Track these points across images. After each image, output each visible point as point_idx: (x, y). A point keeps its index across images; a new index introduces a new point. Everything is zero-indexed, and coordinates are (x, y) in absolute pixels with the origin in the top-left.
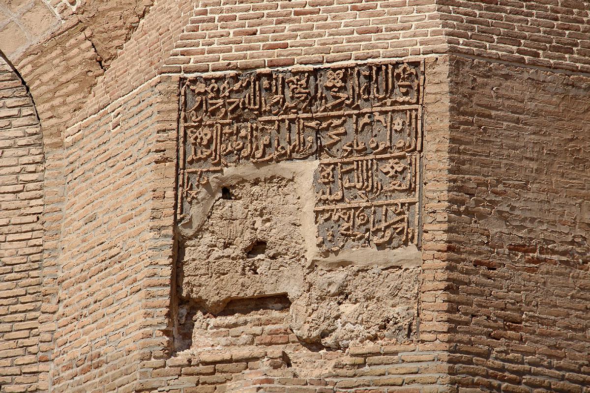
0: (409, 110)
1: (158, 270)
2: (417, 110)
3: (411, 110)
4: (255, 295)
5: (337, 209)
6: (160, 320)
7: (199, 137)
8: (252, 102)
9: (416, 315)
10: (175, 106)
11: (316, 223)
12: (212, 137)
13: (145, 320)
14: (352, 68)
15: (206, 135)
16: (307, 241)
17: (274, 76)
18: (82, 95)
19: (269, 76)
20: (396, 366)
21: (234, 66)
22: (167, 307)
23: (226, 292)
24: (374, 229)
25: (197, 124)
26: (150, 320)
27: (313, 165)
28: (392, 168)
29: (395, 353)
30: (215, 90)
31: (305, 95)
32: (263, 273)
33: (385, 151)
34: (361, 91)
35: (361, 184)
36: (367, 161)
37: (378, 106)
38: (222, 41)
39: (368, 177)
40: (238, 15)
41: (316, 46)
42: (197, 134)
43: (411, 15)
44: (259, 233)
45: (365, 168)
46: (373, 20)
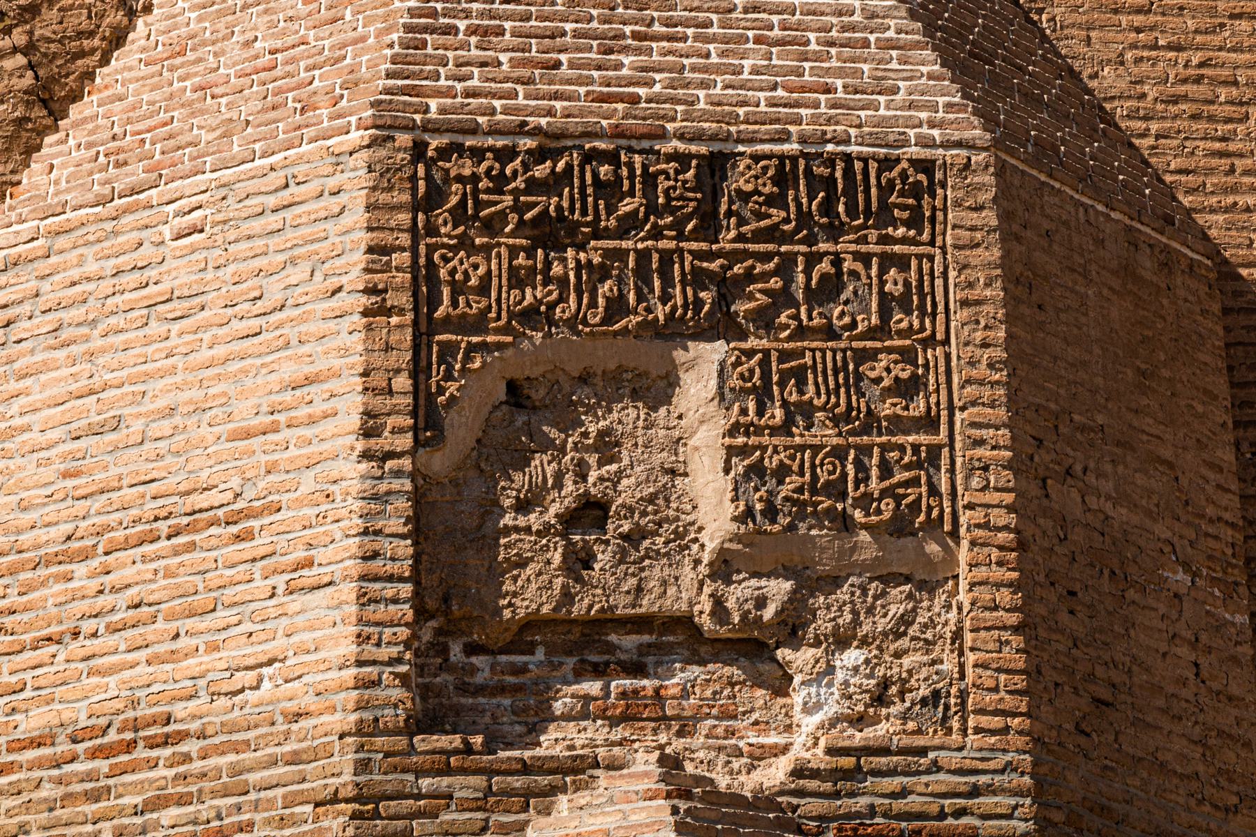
0: (916, 256)
1: (386, 545)
2: (931, 258)
3: (920, 257)
4: (593, 612)
5: (775, 447)
6: (394, 651)
7: (460, 269)
8: (578, 206)
9: (956, 676)
10: (406, 197)
11: (727, 471)
12: (489, 272)
13: (359, 649)
14: (794, 159)
15: (476, 267)
16: (702, 508)
17: (623, 158)
18: (10, 166)
19: (612, 158)
20: (925, 779)
21: (535, 128)
22: (407, 625)
23: (526, 603)
24: (858, 493)
25: (455, 241)
26: (370, 651)
27: (714, 352)
28: (888, 370)
29: (922, 752)
30: (494, 173)
31: (692, 204)
32: (607, 567)
33: (871, 334)
34: (814, 207)
35: (824, 398)
36: (823, 351)
37: (850, 242)
38: (490, 76)
39: (838, 386)
40: (508, 25)
41: (702, 105)
42: (455, 262)
43: (888, 67)
44: (595, 485)
45: (830, 365)
46: (811, 68)
